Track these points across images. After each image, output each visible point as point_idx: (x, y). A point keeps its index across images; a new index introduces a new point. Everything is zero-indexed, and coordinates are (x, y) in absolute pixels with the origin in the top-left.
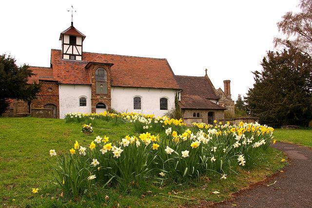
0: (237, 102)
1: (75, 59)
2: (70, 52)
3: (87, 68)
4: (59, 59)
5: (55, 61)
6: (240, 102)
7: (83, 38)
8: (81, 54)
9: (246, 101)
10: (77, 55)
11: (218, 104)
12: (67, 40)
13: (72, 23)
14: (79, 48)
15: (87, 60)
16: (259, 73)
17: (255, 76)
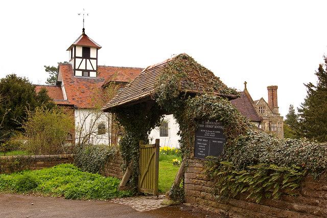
0: (288, 116)
1: (89, 76)
2: (83, 67)
3: (104, 87)
4: (70, 76)
5: (66, 79)
6: (292, 116)
7: (98, 48)
8: (95, 69)
9: (303, 116)
10: (91, 71)
11: (260, 127)
12: (79, 52)
13: (84, 29)
14: (93, 62)
15: (105, 78)
16: (313, 86)
17: (308, 89)
